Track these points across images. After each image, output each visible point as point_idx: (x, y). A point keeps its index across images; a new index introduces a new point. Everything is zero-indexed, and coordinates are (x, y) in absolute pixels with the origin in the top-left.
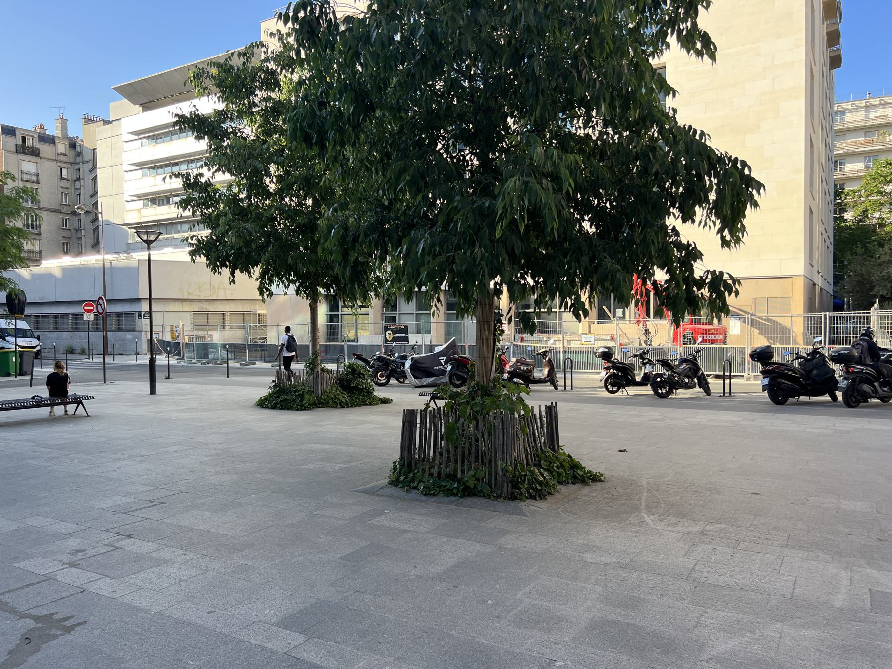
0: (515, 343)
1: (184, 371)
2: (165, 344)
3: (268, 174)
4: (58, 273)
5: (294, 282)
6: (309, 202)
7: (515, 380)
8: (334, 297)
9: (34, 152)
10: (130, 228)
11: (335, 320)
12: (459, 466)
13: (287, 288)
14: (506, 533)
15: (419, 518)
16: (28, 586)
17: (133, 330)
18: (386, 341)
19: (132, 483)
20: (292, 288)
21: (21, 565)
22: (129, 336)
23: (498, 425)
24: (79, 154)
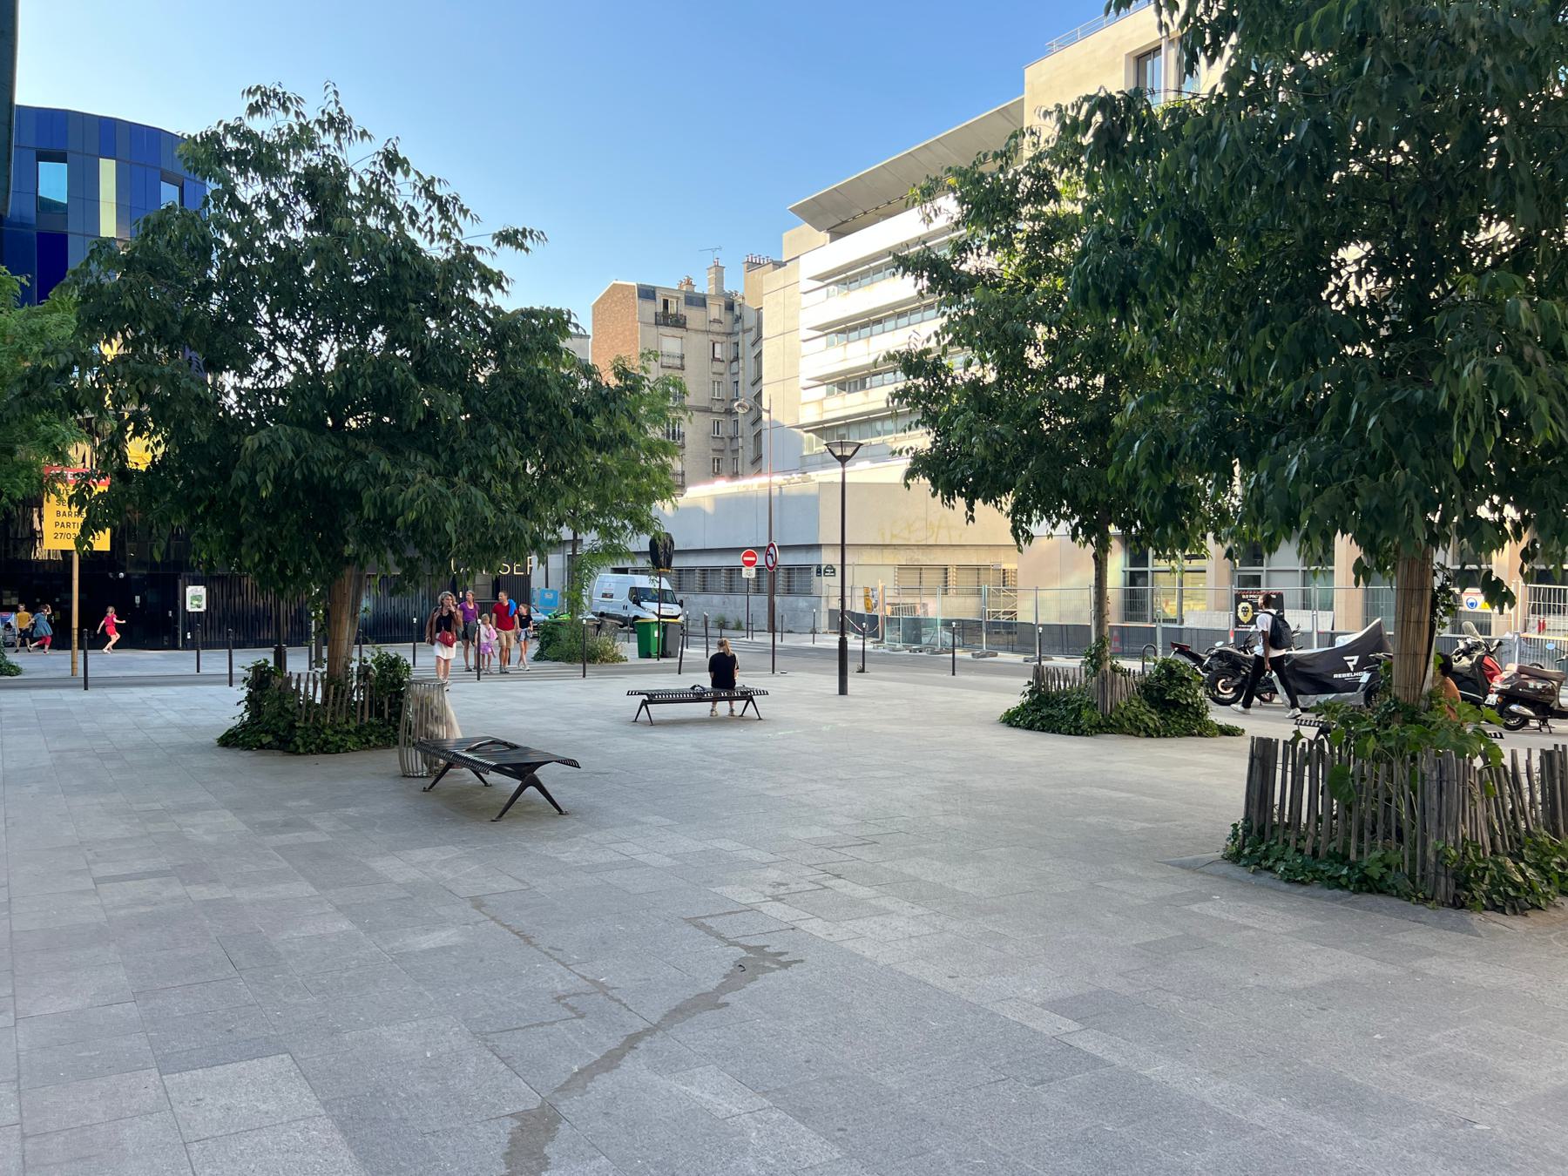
0: (1525, 635)
1: (885, 660)
2: (859, 618)
3: (1032, 341)
4: (709, 507)
5: (1067, 518)
6: (1100, 381)
7: (1514, 708)
8: (1138, 539)
9: (679, 322)
10: (807, 432)
11: (1140, 581)
12: (1353, 841)
13: (1054, 526)
14: (1432, 954)
15: (1274, 912)
16: (730, 913)
17: (809, 594)
18: (1238, 622)
19: (832, 812)
20: (1064, 527)
21: (718, 890)
22: (802, 603)
23: (1431, 775)
24: (738, 319)
